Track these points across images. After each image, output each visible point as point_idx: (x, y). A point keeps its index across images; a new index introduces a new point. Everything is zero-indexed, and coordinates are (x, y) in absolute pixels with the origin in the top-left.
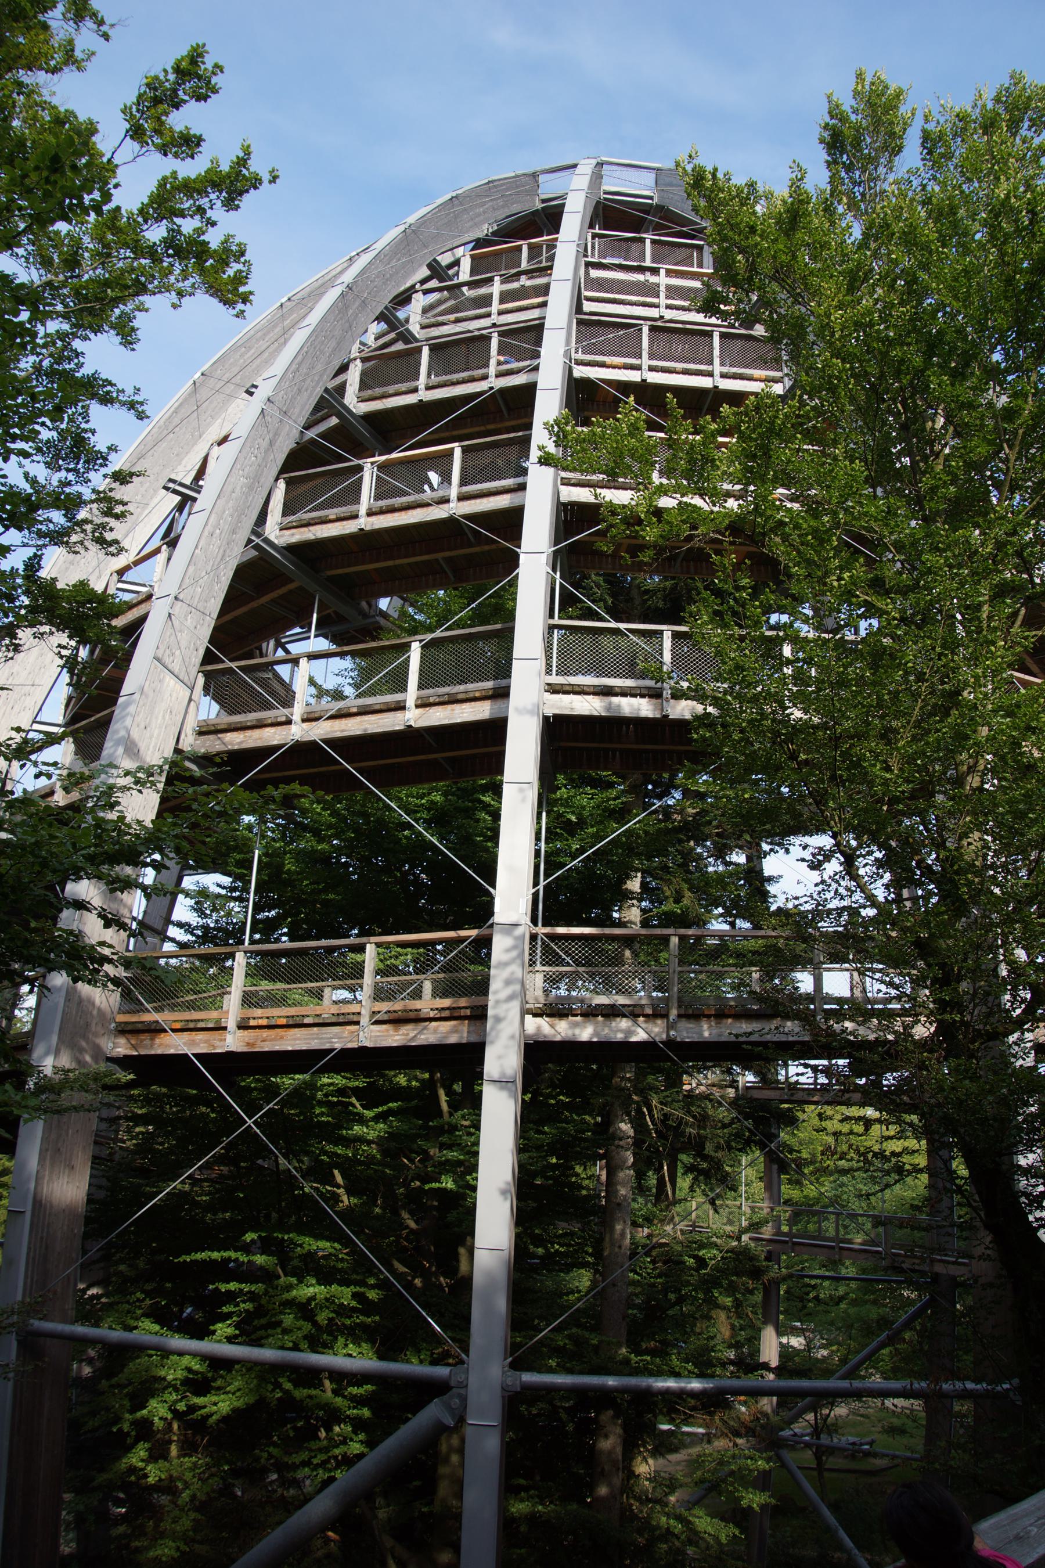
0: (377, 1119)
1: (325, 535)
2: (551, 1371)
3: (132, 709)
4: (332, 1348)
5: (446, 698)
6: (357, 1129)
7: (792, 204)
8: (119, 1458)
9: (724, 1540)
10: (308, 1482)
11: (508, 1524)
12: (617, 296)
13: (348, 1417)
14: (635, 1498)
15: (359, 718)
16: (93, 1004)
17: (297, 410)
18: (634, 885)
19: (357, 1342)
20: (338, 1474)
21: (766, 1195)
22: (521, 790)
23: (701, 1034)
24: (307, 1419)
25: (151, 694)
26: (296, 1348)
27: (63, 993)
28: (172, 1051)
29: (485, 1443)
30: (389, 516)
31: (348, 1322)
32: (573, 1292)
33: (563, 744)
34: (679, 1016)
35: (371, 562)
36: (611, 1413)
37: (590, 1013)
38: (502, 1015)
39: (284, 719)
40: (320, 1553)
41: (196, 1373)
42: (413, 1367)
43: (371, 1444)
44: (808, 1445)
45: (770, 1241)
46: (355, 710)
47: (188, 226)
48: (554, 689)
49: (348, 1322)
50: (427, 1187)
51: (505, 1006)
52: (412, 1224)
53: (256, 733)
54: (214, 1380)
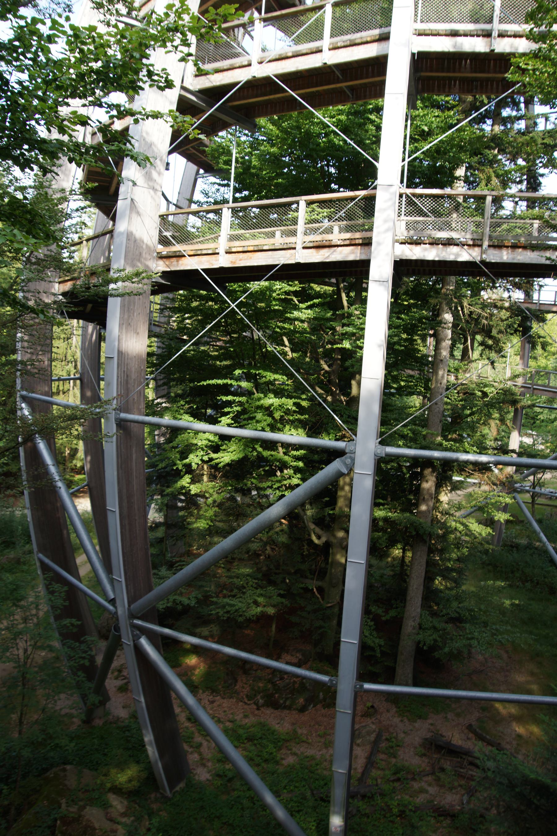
2: (399, 446)
4: (283, 431)
5: (348, 43)
6: (296, 314)
8: (177, 482)
9: (484, 535)
10: (271, 496)
11: (374, 521)
14: (439, 512)
16: (143, 242)
18: (460, 172)
19: (296, 428)
20: (286, 493)
21: (521, 362)
23: (502, 258)
24: (271, 466)
26: (263, 430)
29: (364, 483)
31: (291, 418)
32: (412, 407)
33: (423, 74)
34: (489, 246)
36: (430, 470)
37: (434, 243)
40: (278, 529)
41: (213, 442)
42: (326, 441)
43: (304, 480)
44: (528, 491)
45: (522, 387)
48: (421, 34)
49: (291, 418)
50: (335, 347)
52: (327, 368)
54: (222, 445)
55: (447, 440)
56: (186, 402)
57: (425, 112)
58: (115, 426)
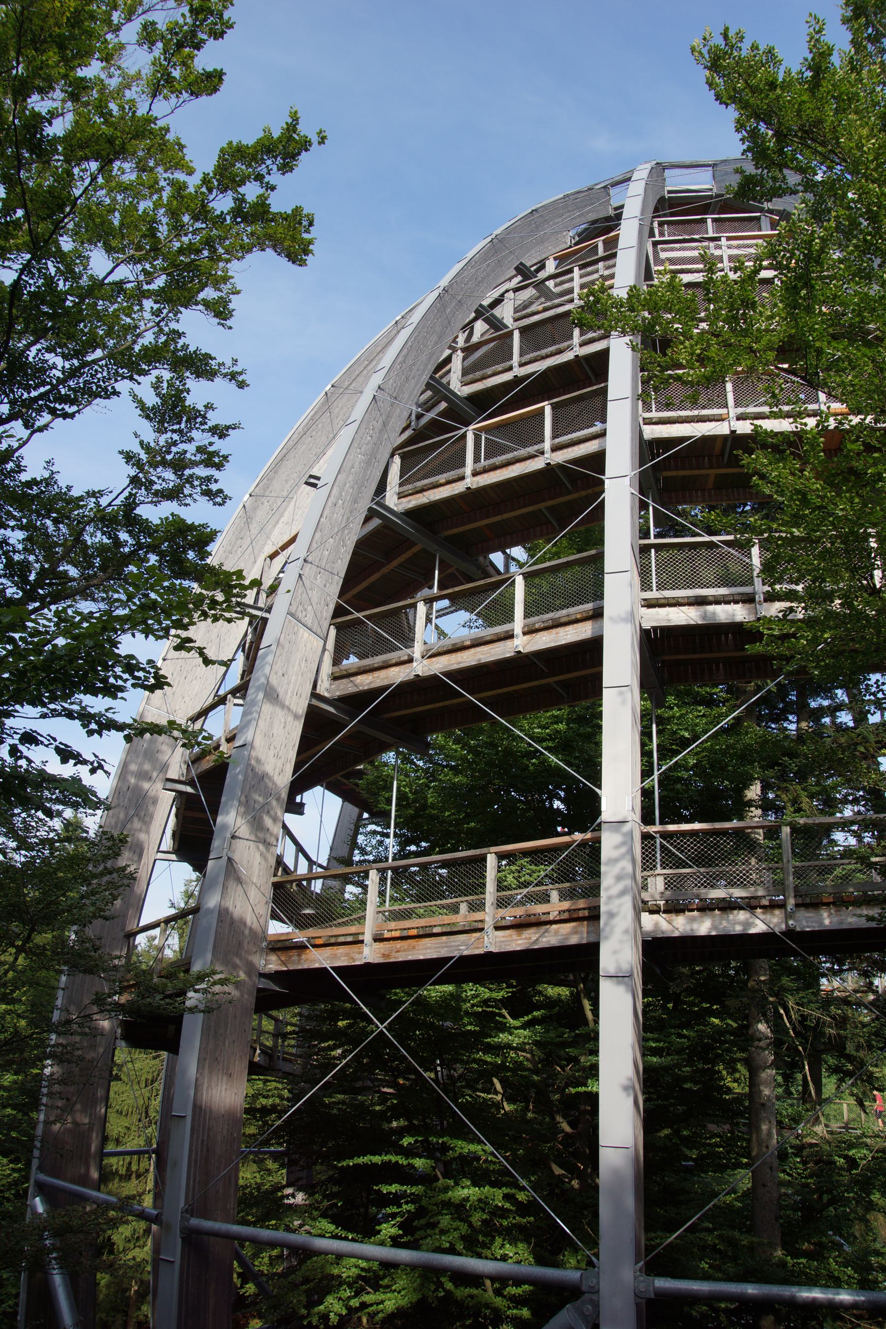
0: (524, 1027)
1: (438, 498)
3: (270, 658)
6: (504, 1037)
7: (813, 59)
12: (684, 267)
13: (508, 1316)
15: (473, 650)
16: (245, 924)
17: (406, 396)
18: (754, 792)
19: (513, 1242)
22: (621, 693)
23: (821, 923)
25: (287, 645)
26: (452, 1250)
27: (216, 915)
28: (317, 965)
30: (492, 474)
31: (505, 1223)
34: (797, 905)
35: (482, 519)
36: (771, 1318)
37: (706, 908)
38: (615, 910)
39: (406, 658)
46: (468, 643)
47: (251, 191)
48: (650, 604)
51: (617, 902)
52: (567, 1128)
53: (382, 674)
55: (796, 1254)
56: (325, 1196)
57: (683, 712)
58: (180, 1240)
